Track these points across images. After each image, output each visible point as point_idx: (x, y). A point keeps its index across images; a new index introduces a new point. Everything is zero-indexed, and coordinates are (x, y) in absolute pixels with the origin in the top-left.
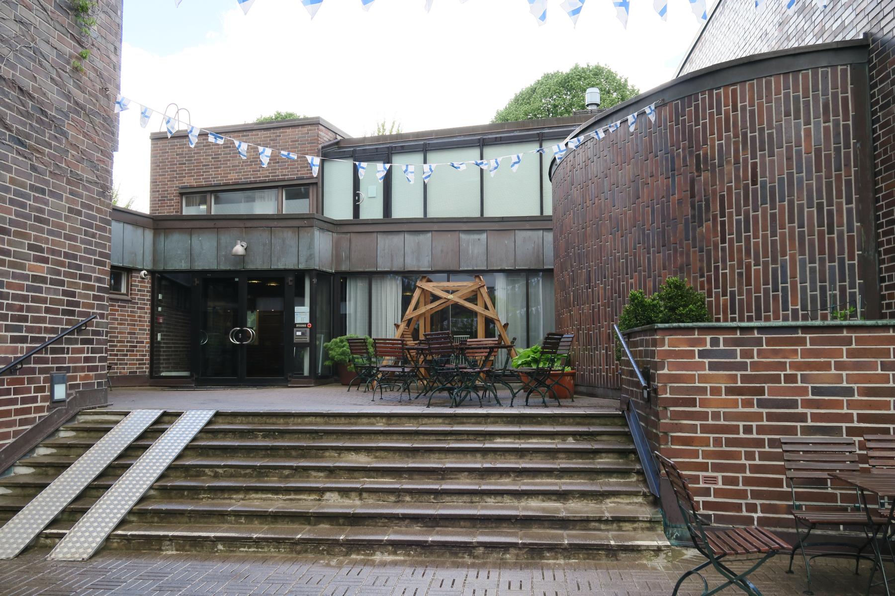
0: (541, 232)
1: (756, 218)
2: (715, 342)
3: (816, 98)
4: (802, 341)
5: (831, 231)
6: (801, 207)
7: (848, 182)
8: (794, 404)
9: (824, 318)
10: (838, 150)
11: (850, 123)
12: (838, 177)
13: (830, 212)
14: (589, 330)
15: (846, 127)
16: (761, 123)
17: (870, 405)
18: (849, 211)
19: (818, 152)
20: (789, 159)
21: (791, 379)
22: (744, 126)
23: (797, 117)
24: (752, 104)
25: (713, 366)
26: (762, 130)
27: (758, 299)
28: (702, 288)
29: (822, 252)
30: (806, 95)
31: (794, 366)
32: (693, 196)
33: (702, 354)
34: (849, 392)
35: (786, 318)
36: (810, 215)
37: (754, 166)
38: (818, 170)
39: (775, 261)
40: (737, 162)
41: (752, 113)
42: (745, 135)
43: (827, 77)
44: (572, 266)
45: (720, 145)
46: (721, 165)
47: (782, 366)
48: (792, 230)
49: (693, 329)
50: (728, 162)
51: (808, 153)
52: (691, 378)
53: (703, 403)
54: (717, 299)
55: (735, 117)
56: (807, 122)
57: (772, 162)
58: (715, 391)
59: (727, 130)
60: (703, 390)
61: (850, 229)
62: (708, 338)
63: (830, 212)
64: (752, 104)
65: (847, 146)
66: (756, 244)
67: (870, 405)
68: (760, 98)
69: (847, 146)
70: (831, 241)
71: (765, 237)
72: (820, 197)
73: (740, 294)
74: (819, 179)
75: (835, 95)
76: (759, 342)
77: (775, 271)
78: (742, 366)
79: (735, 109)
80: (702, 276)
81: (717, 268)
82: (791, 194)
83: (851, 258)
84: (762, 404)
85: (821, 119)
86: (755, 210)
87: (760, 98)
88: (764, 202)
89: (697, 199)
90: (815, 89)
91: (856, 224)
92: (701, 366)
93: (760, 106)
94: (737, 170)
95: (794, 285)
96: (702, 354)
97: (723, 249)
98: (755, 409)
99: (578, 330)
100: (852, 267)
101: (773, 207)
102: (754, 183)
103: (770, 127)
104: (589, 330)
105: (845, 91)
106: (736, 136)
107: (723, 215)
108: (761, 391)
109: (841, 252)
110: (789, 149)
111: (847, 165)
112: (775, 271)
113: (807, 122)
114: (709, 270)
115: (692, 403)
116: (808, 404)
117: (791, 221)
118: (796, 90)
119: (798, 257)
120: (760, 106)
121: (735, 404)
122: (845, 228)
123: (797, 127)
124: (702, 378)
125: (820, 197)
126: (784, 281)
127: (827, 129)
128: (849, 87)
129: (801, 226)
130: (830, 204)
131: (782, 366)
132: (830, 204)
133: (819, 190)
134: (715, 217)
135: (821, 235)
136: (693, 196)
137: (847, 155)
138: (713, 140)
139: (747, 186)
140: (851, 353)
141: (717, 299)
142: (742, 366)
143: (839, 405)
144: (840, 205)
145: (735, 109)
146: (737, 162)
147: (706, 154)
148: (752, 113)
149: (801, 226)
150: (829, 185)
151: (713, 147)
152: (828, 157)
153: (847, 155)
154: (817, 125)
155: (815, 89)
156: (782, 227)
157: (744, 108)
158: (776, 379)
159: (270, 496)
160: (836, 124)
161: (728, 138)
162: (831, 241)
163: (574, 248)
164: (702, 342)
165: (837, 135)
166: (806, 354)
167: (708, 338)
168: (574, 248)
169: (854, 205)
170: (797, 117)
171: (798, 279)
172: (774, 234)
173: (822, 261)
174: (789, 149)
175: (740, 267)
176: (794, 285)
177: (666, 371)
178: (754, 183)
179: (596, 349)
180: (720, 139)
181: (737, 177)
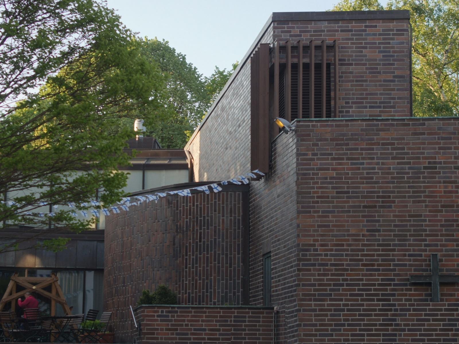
0: (96, 242)
1: (200, 258)
2: (162, 312)
3: (227, 205)
4: (191, 312)
5: (231, 267)
6: (219, 254)
7: (239, 245)
8: (187, 334)
9: (215, 304)
10: (235, 230)
11: (241, 218)
12: (235, 242)
13: (231, 258)
14: (123, 310)
15: (239, 220)
16: (204, 214)
17: (211, 335)
18: (238, 258)
19: (227, 230)
20: (215, 232)
21: (187, 325)
22: (197, 214)
23: (219, 213)
24: (201, 204)
25: (161, 321)
26: (204, 217)
27: (200, 296)
28: (176, 290)
29: (227, 276)
30: (223, 203)
31: (188, 321)
32: (174, 244)
33: (158, 316)
34: (205, 330)
35: (211, 304)
36: (223, 258)
37: (201, 233)
38: (227, 238)
39: (207, 279)
40: (193, 230)
41: (201, 208)
42: (197, 218)
43: (232, 197)
44: (115, 273)
45: (187, 221)
46: (187, 231)
47: (184, 321)
48: (215, 264)
49: (155, 307)
50: (190, 230)
51: (223, 230)
52: (154, 325)
53: (157, 334)
54: (183, 295)
55: (194, 209)
56: (223, 216)
57: (208, 232)
58: (162, 329)
59: (190, 215)
60: (157, 329)
61: (239, 266)
62: (160, 310)
63: (231, 258)
64: (201, 204)
65: (239, 228)
66: (200, 270)
67: (211, 335)
68: (204, 202)
69: (239, 228)
70: (231, 271)
71: (204, 267)
72: (227, 250)
73: (192, 293)
74: (227, 242)
75: (235, 205)
76: (177, 312)
77: (207, 283)
78: (171, 321)
79: (194, 206)
80: (176, 284)
81: (183, 280)
82: (215, 248)
83: (238, 279)
84: (177, 334)
85: (229, 215)
86: (200, 254)
87: (204, 202)
88: (204, 251)
89: (176, 246)
90: (227, 201)
91: (241, 264)
92: (157, 320)
93: (204, 205)
94: (193, 234)
95: (215, 290)
96: (158, 316)
97: (186, 272)
98: (175, 336)
99: (117, 310)
100: (238, 283)
101: (208, 254)
102: (200, 241)
103: (208, 216)
104: (123, 310)
105: (239, 204)
106: (194, 218)
107: (187, 255)
108: (177, 330)
109: (234, 276)
110: (215, 227)
111: (238, 237)
112: (207, 283)
113: (223, 216)
114: (180, 282)
115: (153, 334)
116: (192, 334)
117: (215, 261)
118: (219, 201)
119: (217, 278)
120: (204, 205)
121: (168, 334)
122: (236, 265)
123: (219, 217)
124: (158, 325)
125: (227, 250)
126: (211, 289)
127: (231, 220)
128: (241, 202)
129: (219, 263)
130: (231, 254)
131: (184, 321)
132: (231, 254)
133: (227, 247)
134: (183, 256)
135: (227, 268)
136: (174, 244)
137: (239, 232)
138: (184, 218)
139: (197, 242)
140: (206, 317)
141: (183, 295)
142: (171, 321)
143: (201, 334)
144: (235, 255)
145: (194, 206)
146: (193, 230)
147: (180, 225)
148: (201, 208)
149: (219, 263)
150: (231, 245)
151: (183, 222)
152: (231, 232)
153: (239, 232)
154: (227, 217)
155: (227, 201)
156: (211, 263)
157: (197, 205)
158: (182, 325)
159: (241, 214)
160: (235, 217)
161: (190, 218)
162: (231, 271)
163: (116, 263)
164: (158, 312)
165: (235, 223)
166: (192, 316)
167: (160, 310)
168: (116, 263)
169: (240, 256)
170: (219, 213)
171: (216, 288)
172: (207, 266)
173: (227, 280)
174: (215, 227)
175: (193, 281)
176: (215, 290)
177: (145, 322)
178: (200, 241)
179: (126, 321)
180: (187, 218)
181: (193, 238)
